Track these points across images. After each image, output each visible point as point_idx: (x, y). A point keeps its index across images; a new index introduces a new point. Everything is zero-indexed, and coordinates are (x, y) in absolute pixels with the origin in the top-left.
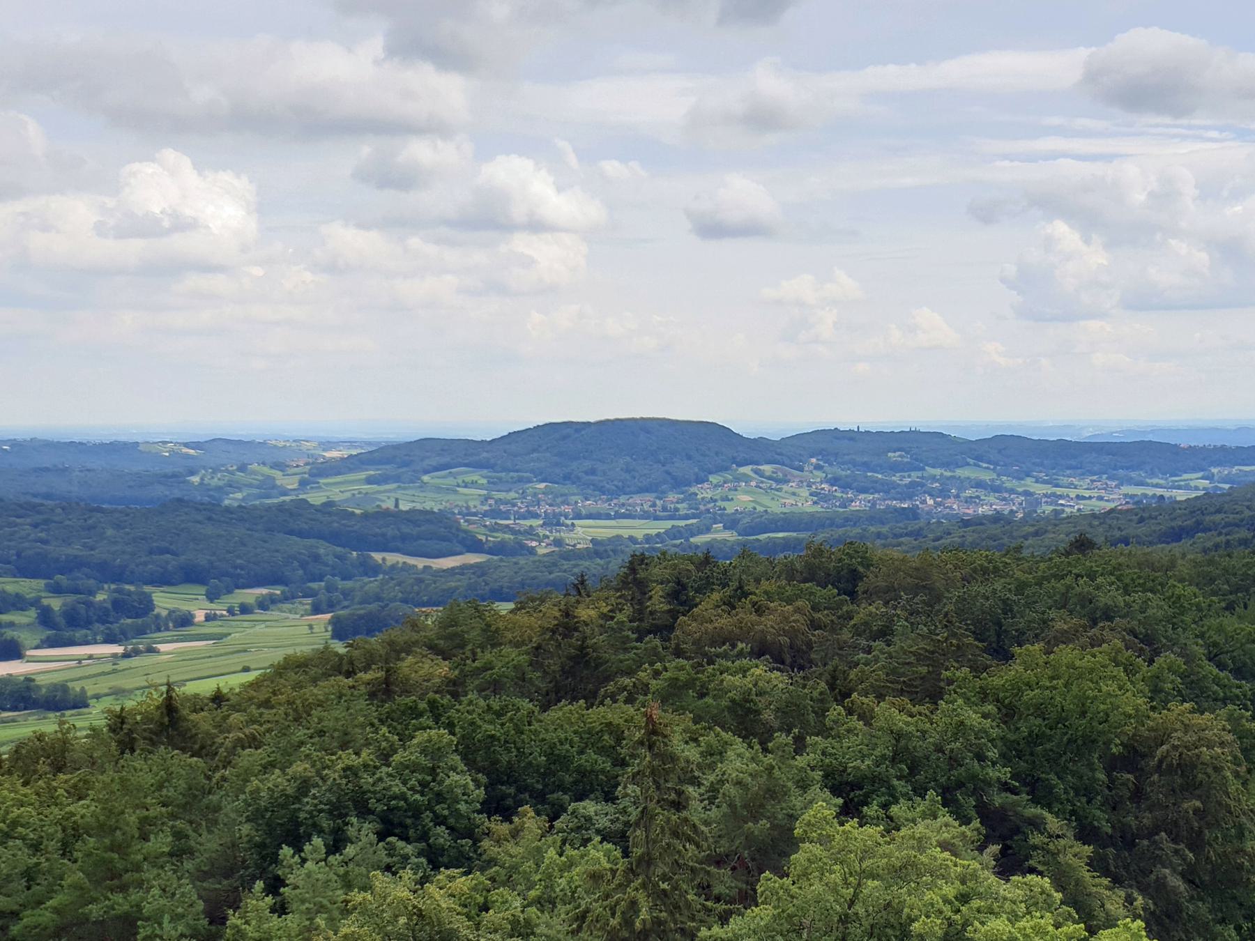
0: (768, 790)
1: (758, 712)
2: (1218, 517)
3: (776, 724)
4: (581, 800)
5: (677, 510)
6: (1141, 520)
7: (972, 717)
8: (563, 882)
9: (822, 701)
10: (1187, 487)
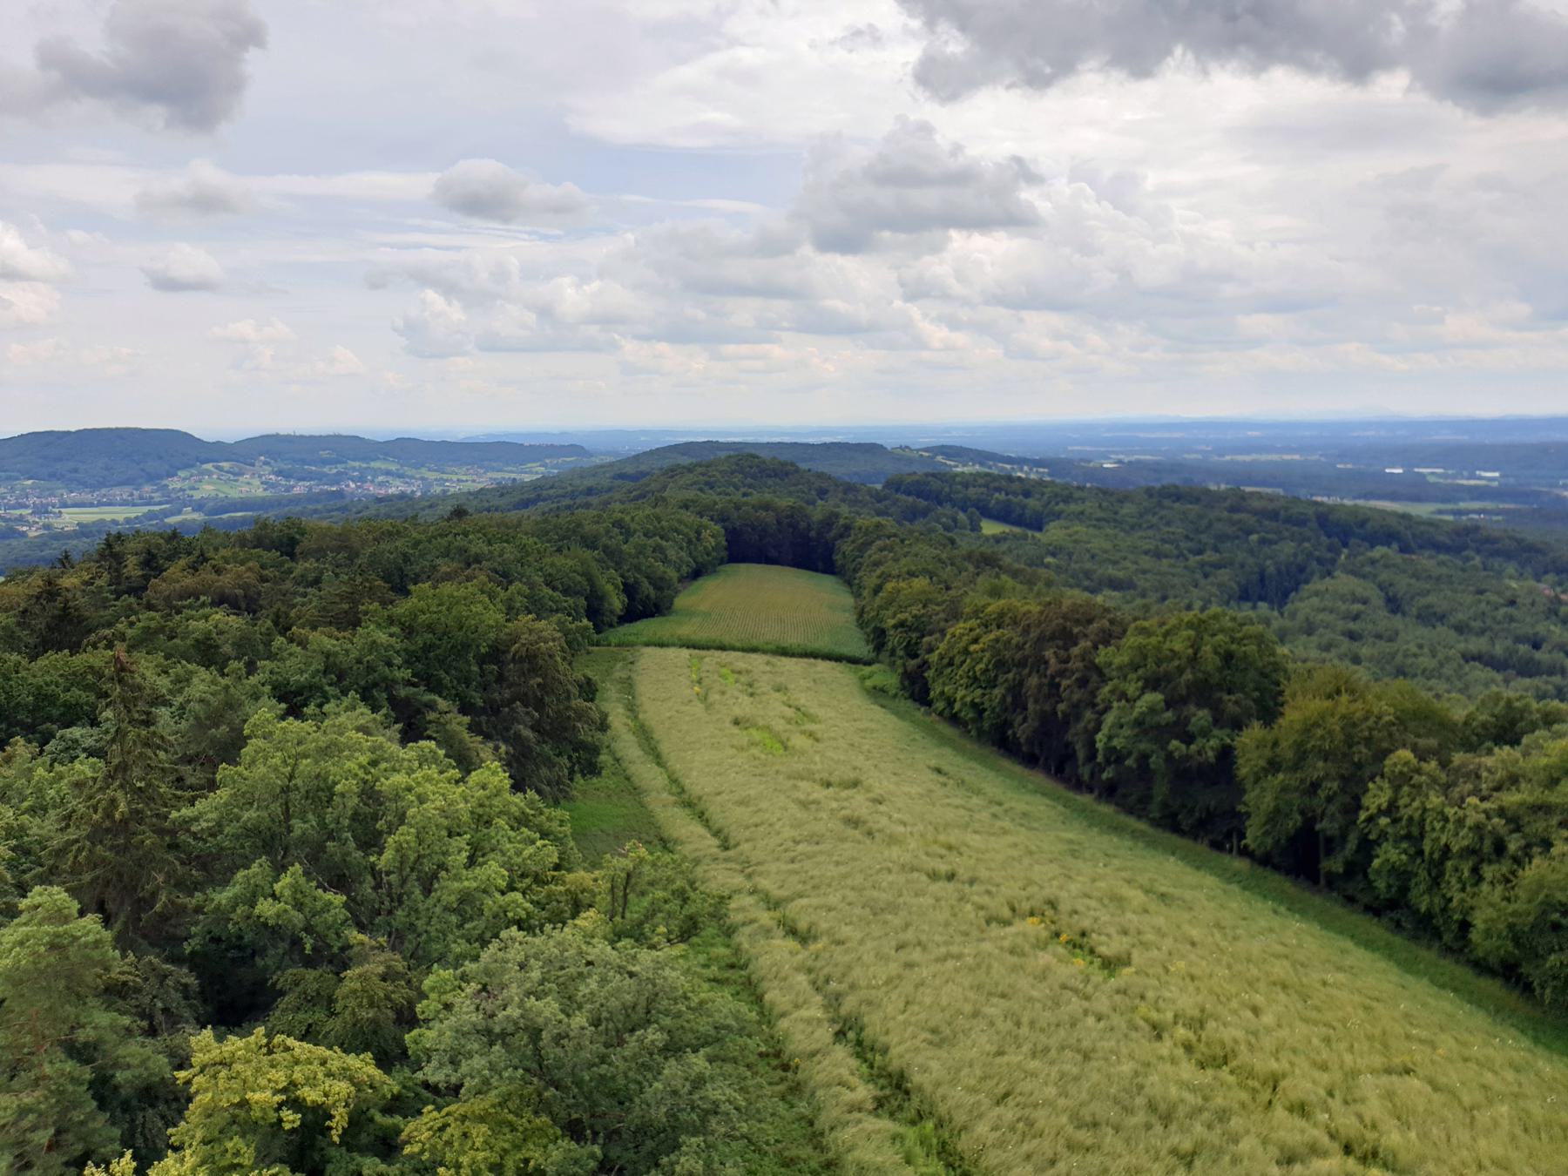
0: (227, 704)
1: (217, 647)
2: (551, 492)
3: (234, 654)
4: (68, 727)
5: (152, 498)
6: (502, 495)
7: (382, 637)
8: (52, 792)
9: (268, 635)
10: (531, 472)
